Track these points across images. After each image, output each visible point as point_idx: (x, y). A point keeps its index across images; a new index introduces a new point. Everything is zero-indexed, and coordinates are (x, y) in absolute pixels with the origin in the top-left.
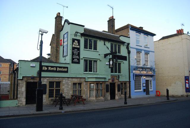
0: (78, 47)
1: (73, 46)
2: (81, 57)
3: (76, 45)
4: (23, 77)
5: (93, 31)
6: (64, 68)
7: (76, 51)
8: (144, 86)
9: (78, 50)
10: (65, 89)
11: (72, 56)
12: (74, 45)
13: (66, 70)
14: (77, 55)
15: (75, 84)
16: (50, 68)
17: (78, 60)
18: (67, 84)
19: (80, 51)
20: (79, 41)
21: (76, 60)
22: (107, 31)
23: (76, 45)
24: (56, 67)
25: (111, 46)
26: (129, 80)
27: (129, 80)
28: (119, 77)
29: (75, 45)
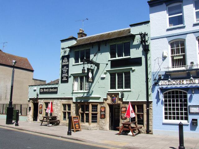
0: (67, 63)
1: (63, 63)
2: (70, 73)
6: (55, 88)
8: (116, 109)
9: (67, 68)
11: (62, 75)
12: (64, 62)
13: (55, 90)
15: (64, 105)
16: (45, 90)
17: (66, 78)
18: (57, 105)
19: (69, 68)
21: (65, 79)
22: (124, 93)
24: (49, 88)
26: (146, 100)
27: (146, 100)
28: (123, 96)
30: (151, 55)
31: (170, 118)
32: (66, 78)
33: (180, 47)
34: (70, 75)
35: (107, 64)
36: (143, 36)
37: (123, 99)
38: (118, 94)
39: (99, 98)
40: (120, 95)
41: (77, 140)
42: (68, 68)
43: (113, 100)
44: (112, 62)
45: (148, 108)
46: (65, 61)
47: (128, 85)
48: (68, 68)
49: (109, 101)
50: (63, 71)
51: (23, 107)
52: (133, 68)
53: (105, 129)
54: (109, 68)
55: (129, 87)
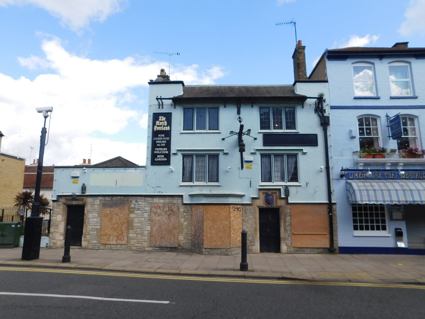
0: (168, 128)
3: (161, 126)
4: (59, 196)
5: (405, 57)
7: (161, 139)
9: (165, 137)
10: (136, 220)
11: (153, 149)
12: (158, 126)
14: (163, 147)
17: (165, 157)
20: (168, 116)
21: (160, 158)
23: (161, 126)
25: (395, 106)
27: (326, 201)
29: (159, 126)
30: (331, 130)
31: (362, 229)
32: (163, 156)
33: (289, 125)
34: (173, 151)
35: (255, 139)
36: (320, 99)
37: (289, 198)
38: (279, 190)
39: (241, 196)
40: (282, 191)
41: (350, 281)
42: (168, 139)
43: (267, 201)
44: (265, 136)
45: (331, 213)
46: (161, 123)
47: (294, 177)
48: (168, 139)
49: (261, 203)
50: (157, 142)
51: (5, 212)
52: (306, 149)
53: (253, 252)
54: (259, 144)
55: (217, 181)
